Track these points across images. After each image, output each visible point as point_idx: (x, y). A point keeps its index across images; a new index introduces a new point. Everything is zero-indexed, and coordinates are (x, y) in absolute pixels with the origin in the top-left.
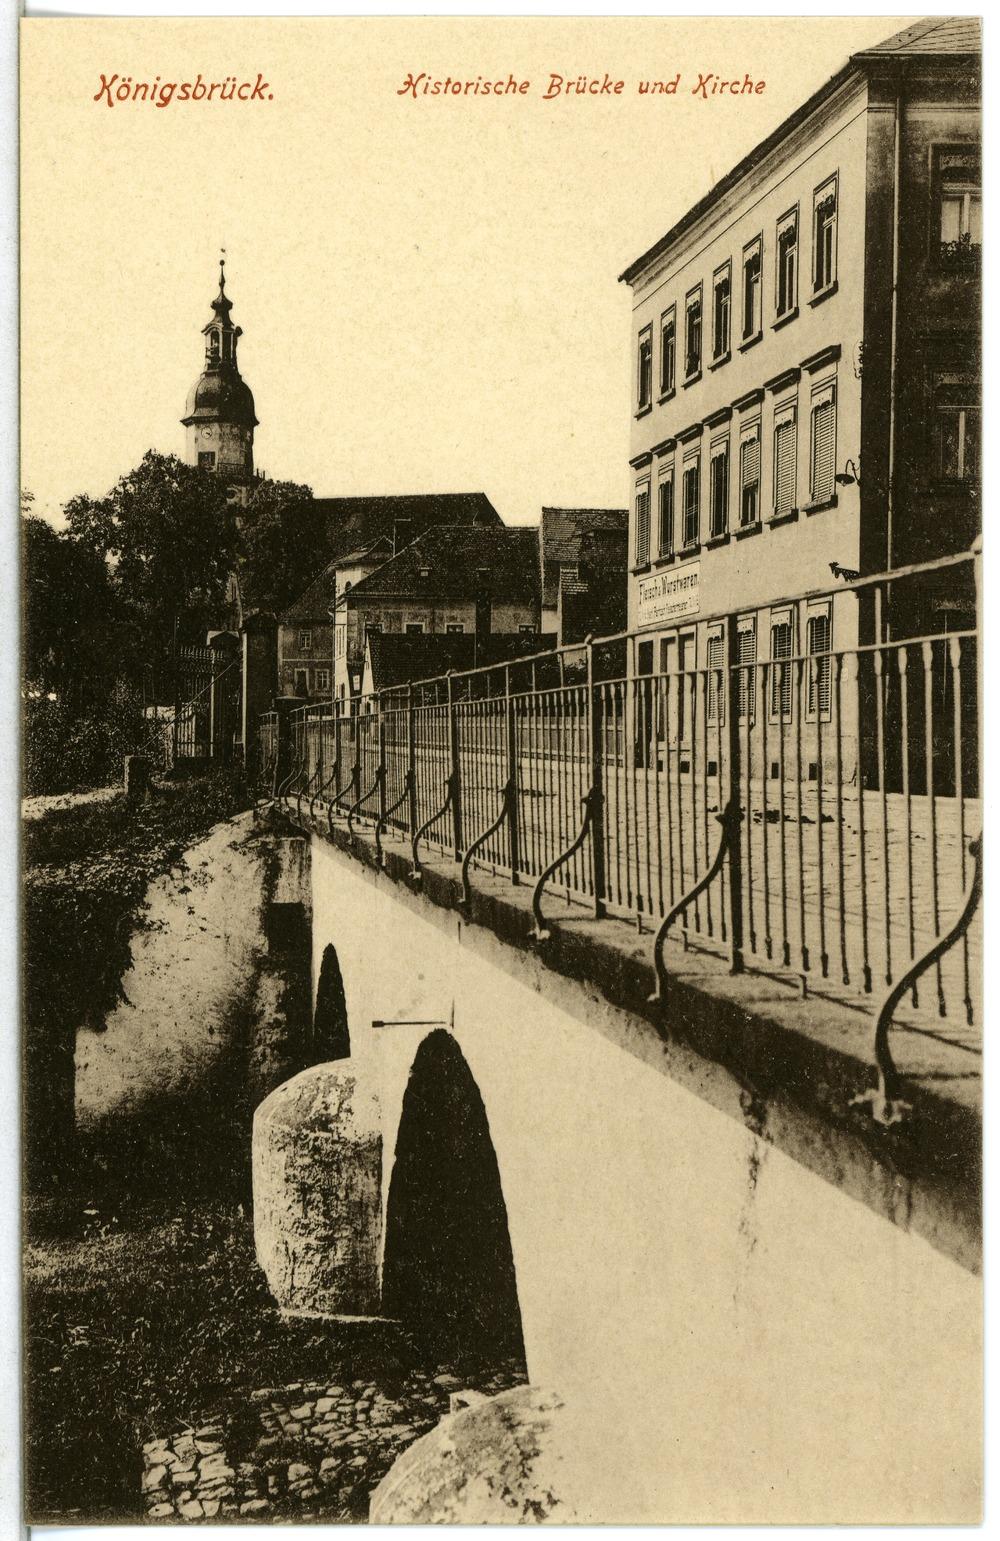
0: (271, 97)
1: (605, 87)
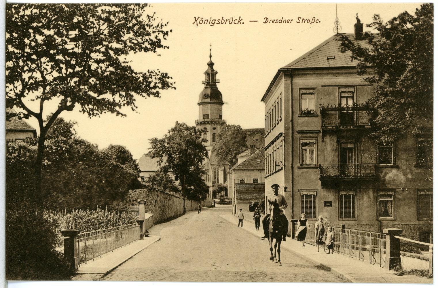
0: (243, 23)
1: (239, 21)
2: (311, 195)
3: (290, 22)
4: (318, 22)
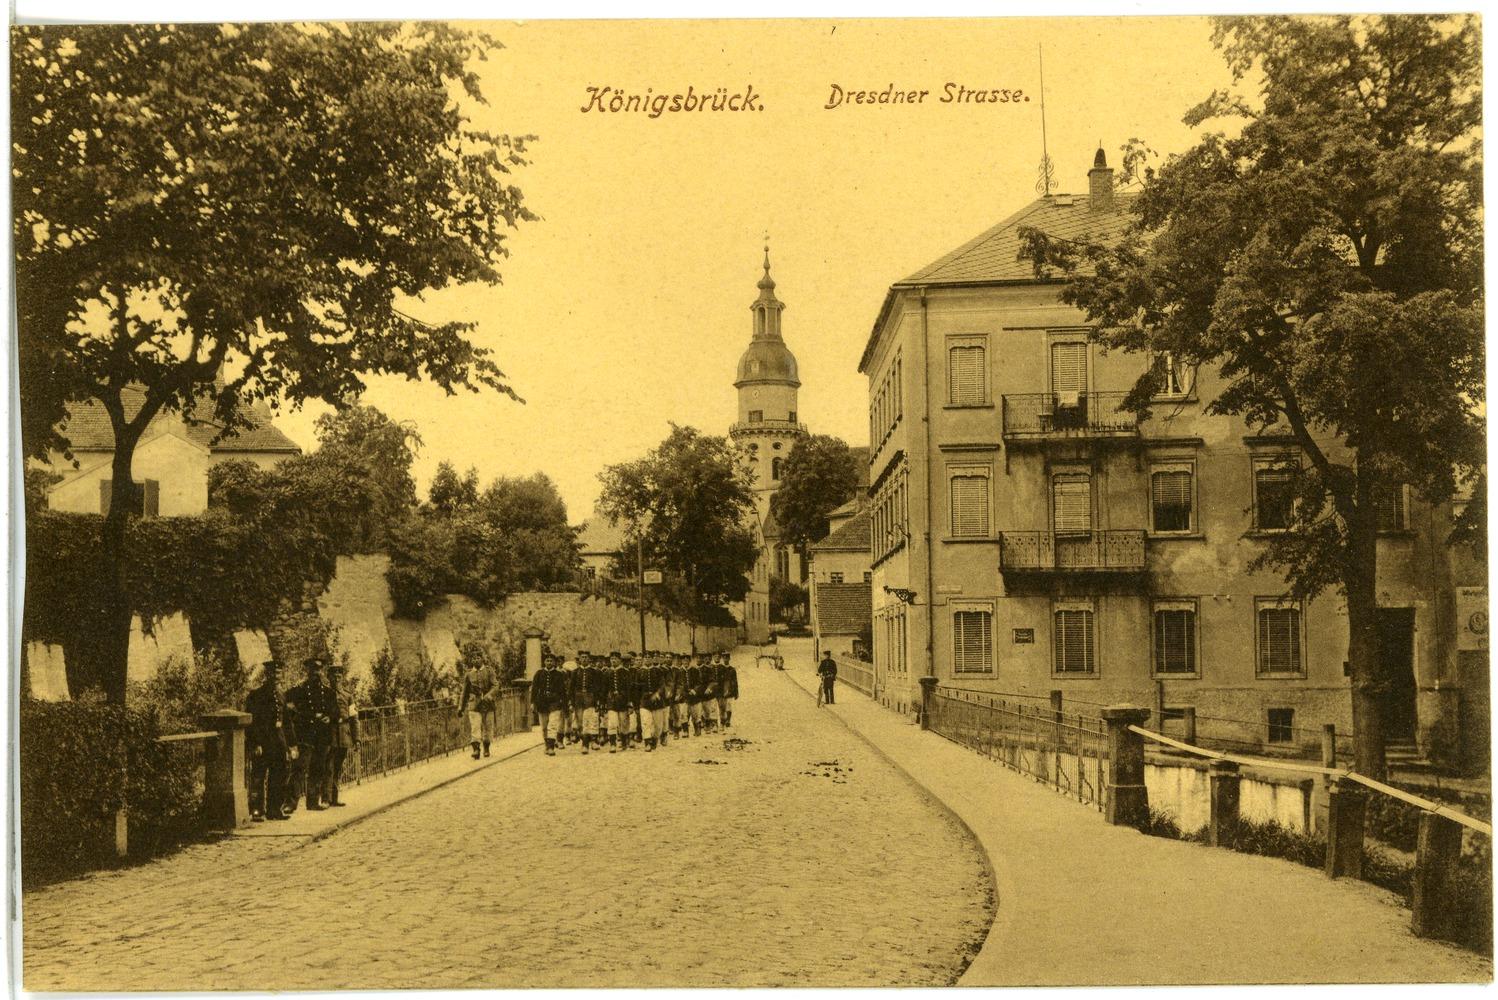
0: (761, 108)
2: (978, 614)
3: (916, 99)
4: (1022, 98)
